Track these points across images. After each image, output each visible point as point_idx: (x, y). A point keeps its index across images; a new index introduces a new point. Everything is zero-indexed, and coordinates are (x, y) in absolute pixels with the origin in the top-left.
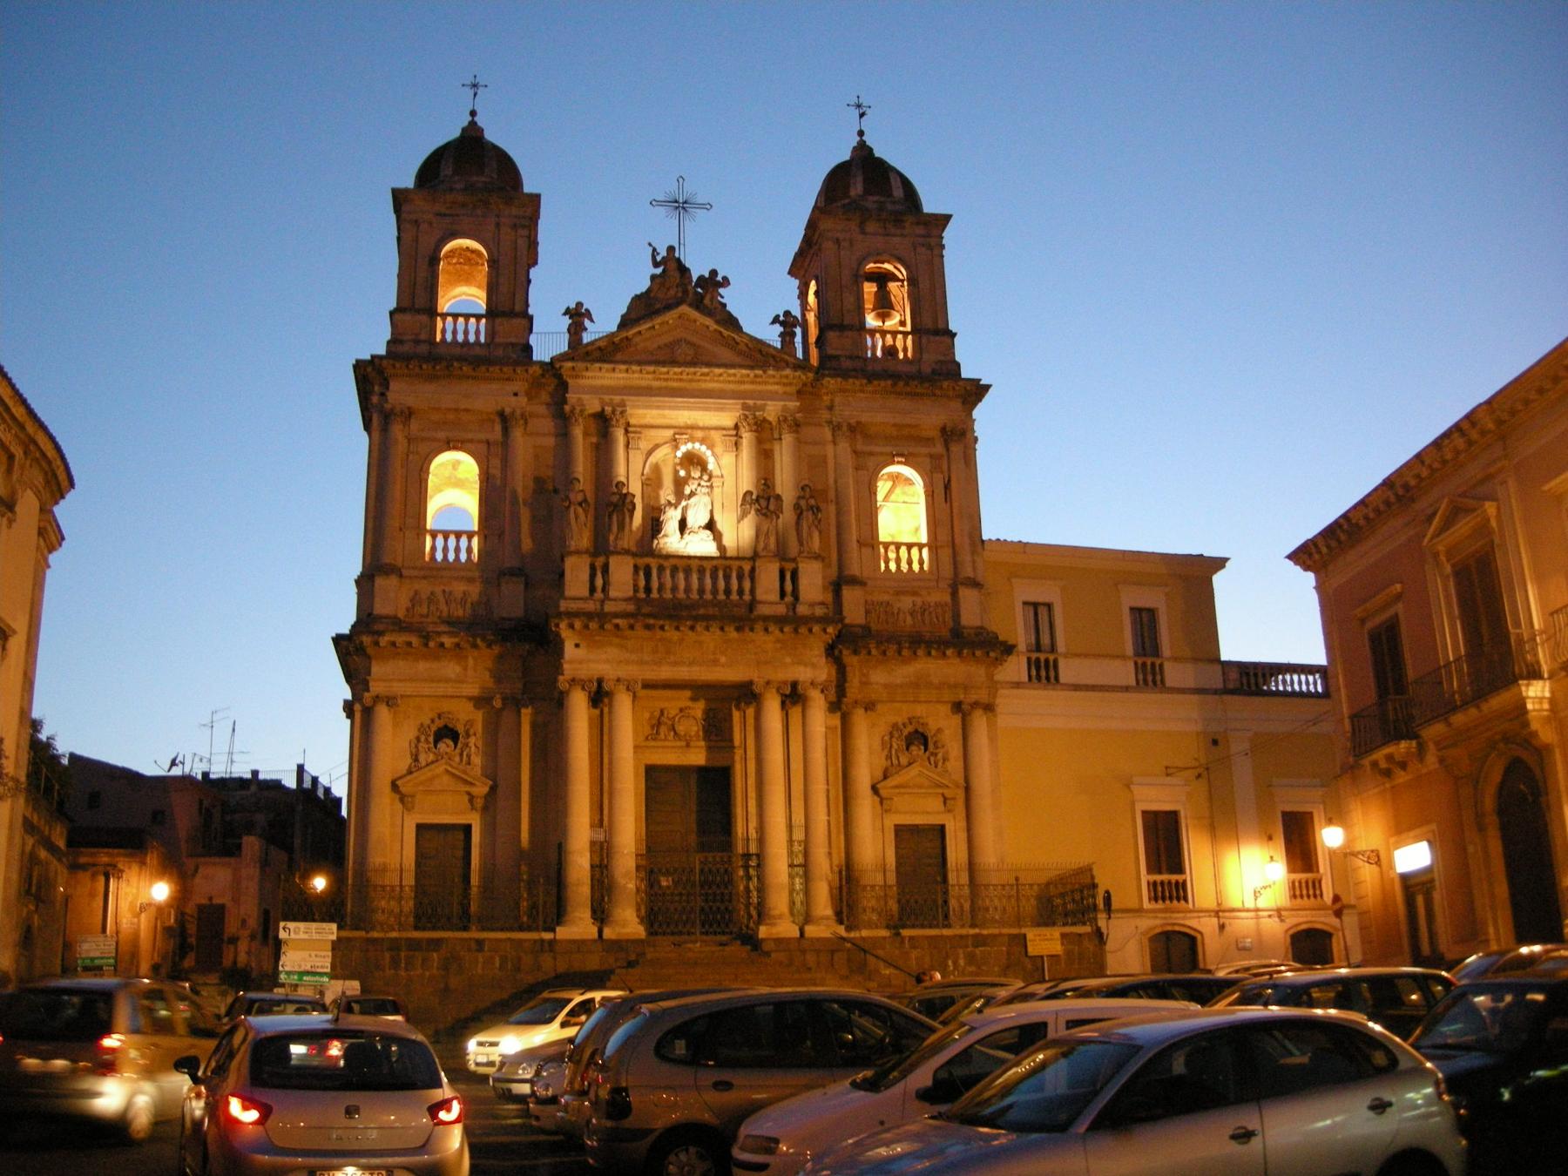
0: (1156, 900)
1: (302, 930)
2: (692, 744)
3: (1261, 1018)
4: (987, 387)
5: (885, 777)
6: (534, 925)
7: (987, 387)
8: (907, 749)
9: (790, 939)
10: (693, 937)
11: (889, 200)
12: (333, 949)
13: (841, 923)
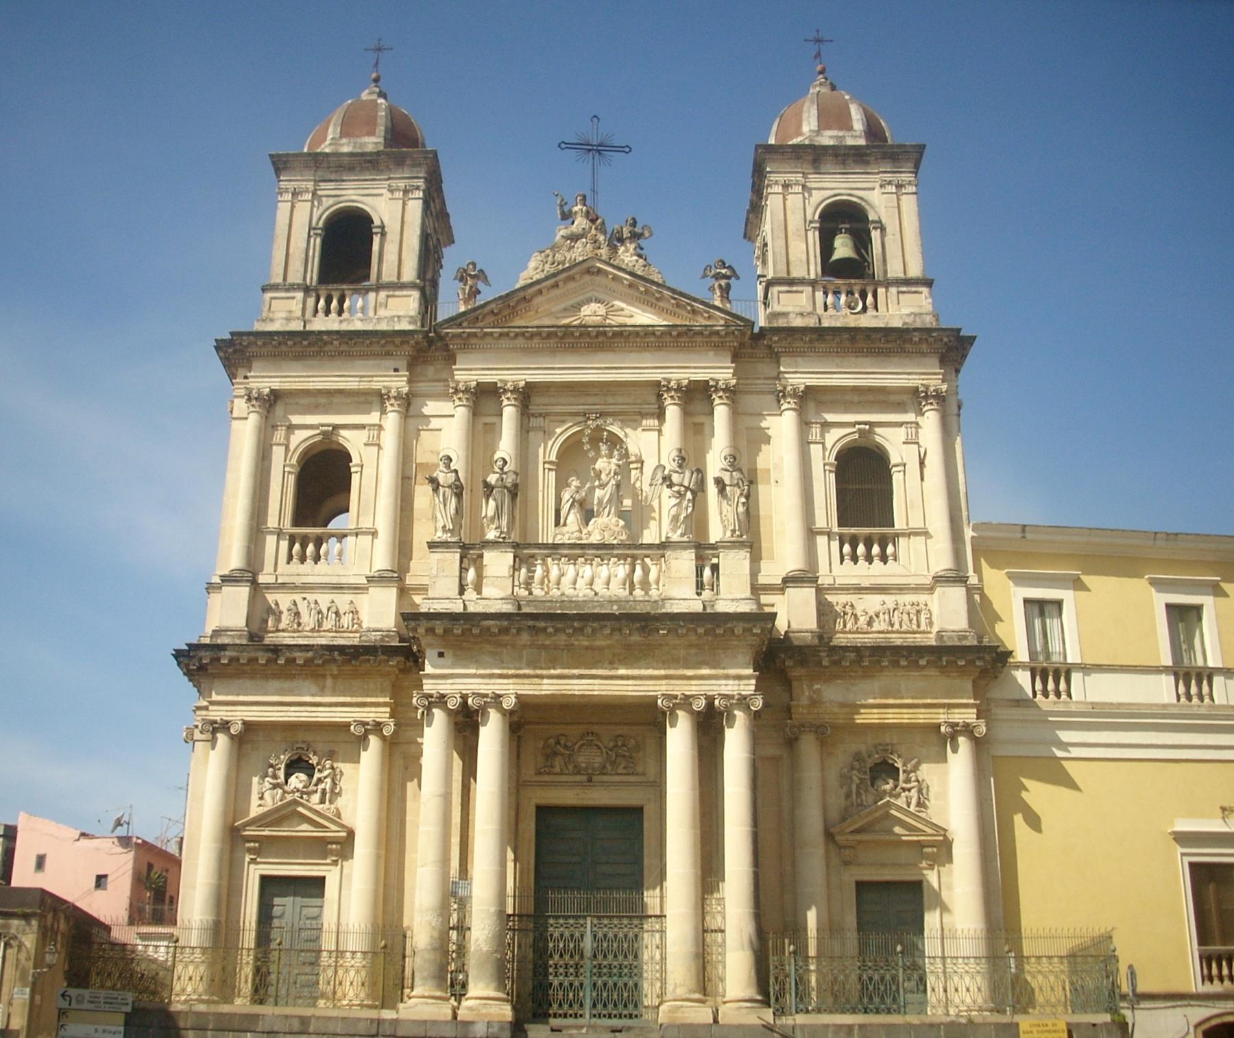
0: (1211, 980)
1: (87, 998)
2: (595, 778)
3: (868, 413)
4: (971, 339)
5: (843, 819)
6: (895, 1007)
7: (971, 339)
8: (872, 785)
9: (699, 1026)
10: (580, 1021)
11: (850, 133)
12: (127, 1024)
13: (766, 1003)
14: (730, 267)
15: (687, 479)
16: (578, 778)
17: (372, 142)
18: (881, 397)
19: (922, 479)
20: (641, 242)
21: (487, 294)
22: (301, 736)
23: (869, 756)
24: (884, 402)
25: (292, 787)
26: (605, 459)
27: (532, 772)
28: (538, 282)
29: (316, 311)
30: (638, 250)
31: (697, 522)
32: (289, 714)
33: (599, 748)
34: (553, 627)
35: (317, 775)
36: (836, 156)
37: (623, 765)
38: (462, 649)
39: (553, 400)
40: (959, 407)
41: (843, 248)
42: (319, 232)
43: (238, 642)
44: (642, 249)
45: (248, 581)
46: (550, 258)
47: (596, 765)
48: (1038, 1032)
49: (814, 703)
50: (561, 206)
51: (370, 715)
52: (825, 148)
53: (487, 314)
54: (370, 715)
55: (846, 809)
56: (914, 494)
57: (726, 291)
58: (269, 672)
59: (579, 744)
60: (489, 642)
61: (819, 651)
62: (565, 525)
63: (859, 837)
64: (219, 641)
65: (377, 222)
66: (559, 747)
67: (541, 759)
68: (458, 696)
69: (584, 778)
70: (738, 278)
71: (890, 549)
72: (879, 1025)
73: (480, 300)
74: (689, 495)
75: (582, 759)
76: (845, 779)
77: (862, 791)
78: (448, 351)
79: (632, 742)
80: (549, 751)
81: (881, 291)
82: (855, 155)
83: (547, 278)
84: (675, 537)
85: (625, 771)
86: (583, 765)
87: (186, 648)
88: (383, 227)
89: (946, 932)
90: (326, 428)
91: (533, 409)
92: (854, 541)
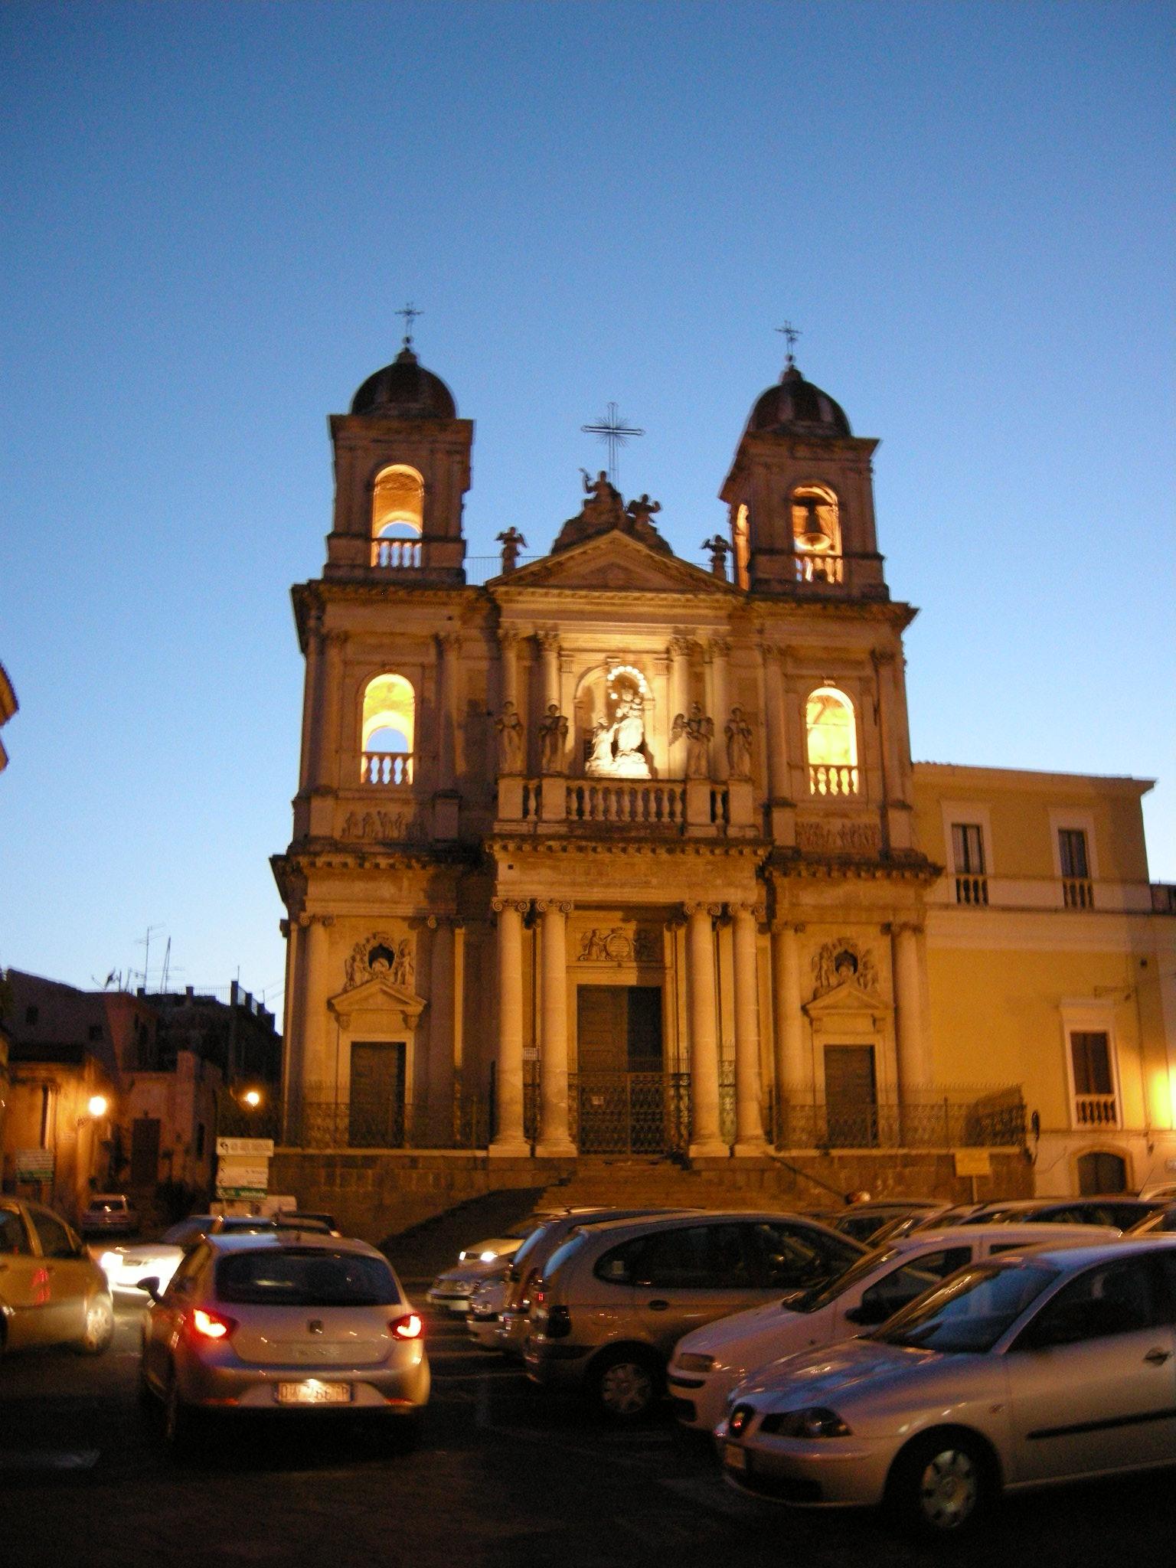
5: (815, 998)
13: (771, 1142)
16: (610, 964)
19: (170, 939)
35: (396, 959)
59: (610, 937)
69: (615, 964)
72: (853, 1157)
76: (816, 966)
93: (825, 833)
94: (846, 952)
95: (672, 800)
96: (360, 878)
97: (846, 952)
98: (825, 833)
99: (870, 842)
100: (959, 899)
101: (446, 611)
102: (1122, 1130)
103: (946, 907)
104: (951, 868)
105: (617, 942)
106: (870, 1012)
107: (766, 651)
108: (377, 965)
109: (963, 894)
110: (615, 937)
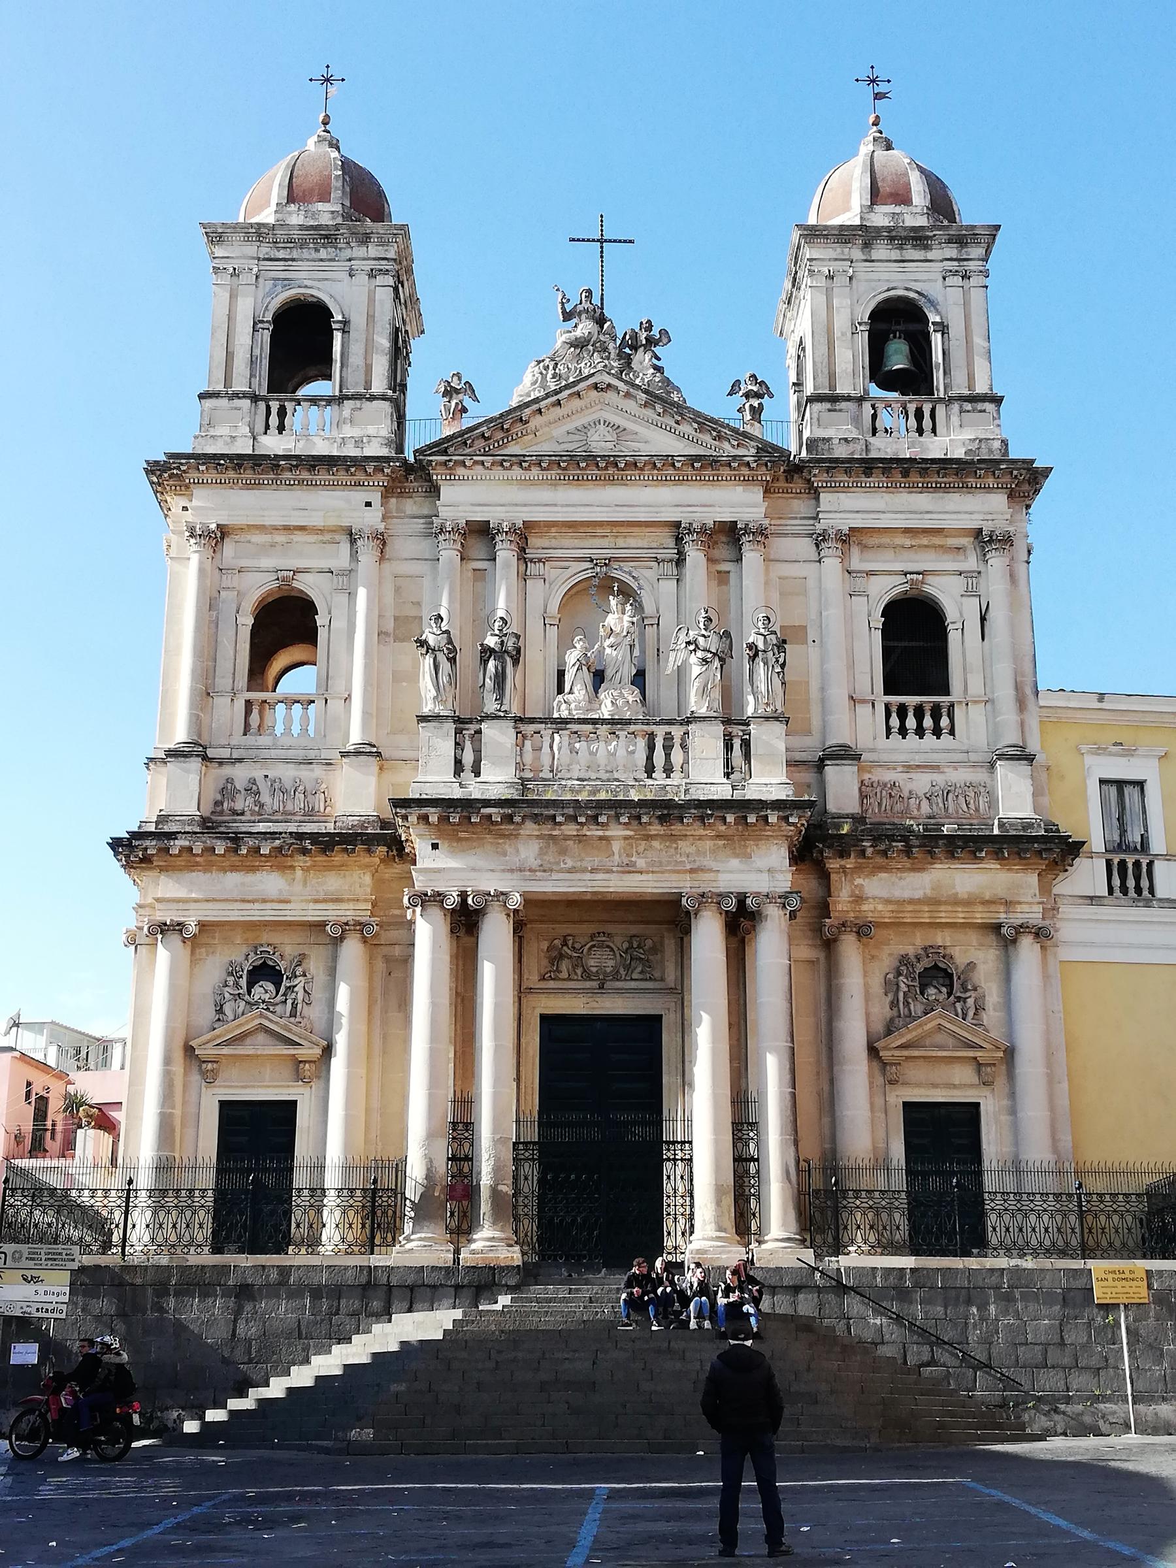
4: (1047, 471)
5: (889, 1032)
7: (1047, 471)
14: (762, 383)
15: (713, 644)
16: (588, 984)
17: (326, 212)
18: (937, 541)
19: (983, 639)
20: (657, 350)
21: (477, 413)
22: (266, 937)
23: (919, 960)
24: (941, 546)
25: (256, 998)
26: (616, 616)
27: (536, 978)
28: (536, 401)
29: (267, 427)
30: (655, 361)
31: (729, 696)
32: (252, 913)
33: (612, 950)
34: (563, 815)
35: (285, 983)
36: (892, 239)
37: (639, 969)
38: (460, 840)
39: (554, 543)
40: (1029, 552)
41: (898, 358)
42: (266, 326)
43: (188, 829)
44: (658, 359)
45: (197, 756)
46: (551, 372)
47: (608, 970)
48: (1114, 1279)
49: (859, 899)
50: (563, 304)
51: (348, 913)
52: (878, 229)
53: (477, 438)
54: (348, 913)
55: (892, 1020)
56: (974, 658)
57: (756, 412)
58: (228, 863)
59: (588, 946)
60: (490, 832)
61: (862, 841)
62: (571, 692)
63: (906, 1053)
64: (166, 829)
65: (338, 317)
66: (565, 948)
67: (545, 962)
68: (455, 894)
69: (595, 984)
70: (771, 396)
71: (944, 722)
73: (467, 422)
74: (717, 663)
75: (592, 963)
76: (890, 986)
77: (910, 1000)
78: (430, 480)
79: (649, 943)
80: (554, 954)
81: (941, 410)
82: (913, 238)
83: (547, 396)
84: (703, 711)
85: (641, 976)
86: (594, 970)
87: (128, 836)
88: (345, 322)
89: (704, 761)
90: (285, 573)
91: (531, 553)
92: (902, 711)
93: (906, 794)
94: (936, 967)
95: (668, 749)
96: (234, 868)
97: (936, 967)
98: (906, 794)
99: (972, 806)
100: (1111, 890)
101: (361, 496)
102: (375, 1284)
103: (1092, 900)
104: (1097, 843)
105: (598, 953)
106: (971, 1054)
107: (820, 540)
108: (257, 991)
109: (1116, 882)
110: (594, 946)
